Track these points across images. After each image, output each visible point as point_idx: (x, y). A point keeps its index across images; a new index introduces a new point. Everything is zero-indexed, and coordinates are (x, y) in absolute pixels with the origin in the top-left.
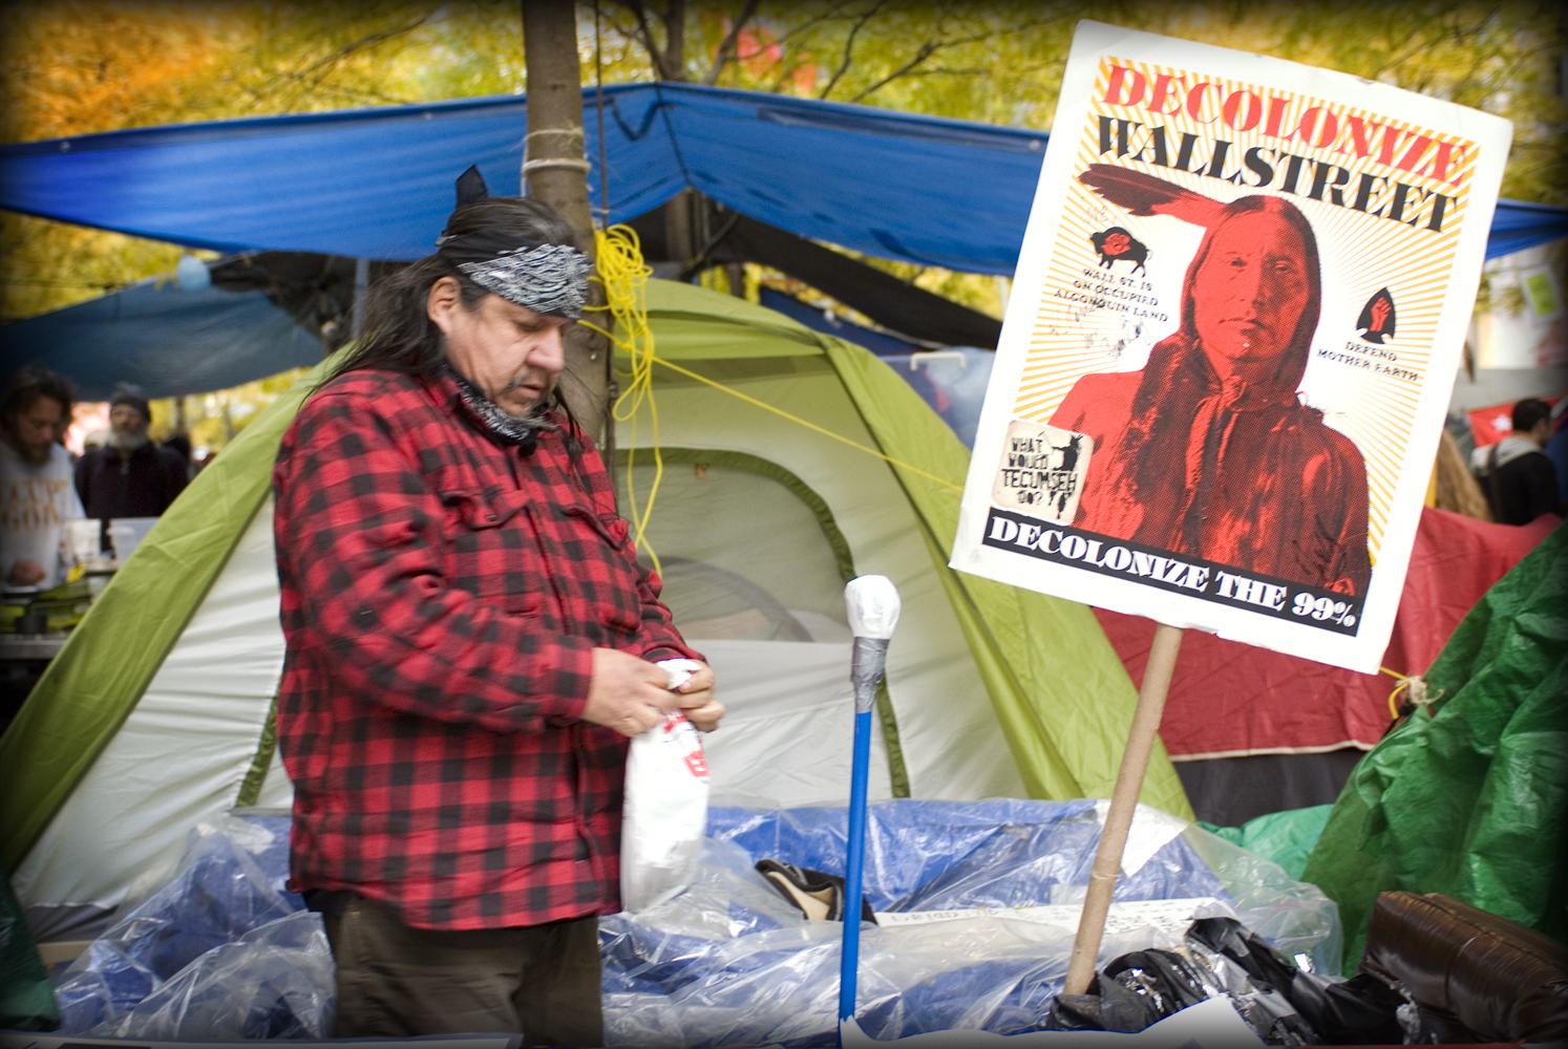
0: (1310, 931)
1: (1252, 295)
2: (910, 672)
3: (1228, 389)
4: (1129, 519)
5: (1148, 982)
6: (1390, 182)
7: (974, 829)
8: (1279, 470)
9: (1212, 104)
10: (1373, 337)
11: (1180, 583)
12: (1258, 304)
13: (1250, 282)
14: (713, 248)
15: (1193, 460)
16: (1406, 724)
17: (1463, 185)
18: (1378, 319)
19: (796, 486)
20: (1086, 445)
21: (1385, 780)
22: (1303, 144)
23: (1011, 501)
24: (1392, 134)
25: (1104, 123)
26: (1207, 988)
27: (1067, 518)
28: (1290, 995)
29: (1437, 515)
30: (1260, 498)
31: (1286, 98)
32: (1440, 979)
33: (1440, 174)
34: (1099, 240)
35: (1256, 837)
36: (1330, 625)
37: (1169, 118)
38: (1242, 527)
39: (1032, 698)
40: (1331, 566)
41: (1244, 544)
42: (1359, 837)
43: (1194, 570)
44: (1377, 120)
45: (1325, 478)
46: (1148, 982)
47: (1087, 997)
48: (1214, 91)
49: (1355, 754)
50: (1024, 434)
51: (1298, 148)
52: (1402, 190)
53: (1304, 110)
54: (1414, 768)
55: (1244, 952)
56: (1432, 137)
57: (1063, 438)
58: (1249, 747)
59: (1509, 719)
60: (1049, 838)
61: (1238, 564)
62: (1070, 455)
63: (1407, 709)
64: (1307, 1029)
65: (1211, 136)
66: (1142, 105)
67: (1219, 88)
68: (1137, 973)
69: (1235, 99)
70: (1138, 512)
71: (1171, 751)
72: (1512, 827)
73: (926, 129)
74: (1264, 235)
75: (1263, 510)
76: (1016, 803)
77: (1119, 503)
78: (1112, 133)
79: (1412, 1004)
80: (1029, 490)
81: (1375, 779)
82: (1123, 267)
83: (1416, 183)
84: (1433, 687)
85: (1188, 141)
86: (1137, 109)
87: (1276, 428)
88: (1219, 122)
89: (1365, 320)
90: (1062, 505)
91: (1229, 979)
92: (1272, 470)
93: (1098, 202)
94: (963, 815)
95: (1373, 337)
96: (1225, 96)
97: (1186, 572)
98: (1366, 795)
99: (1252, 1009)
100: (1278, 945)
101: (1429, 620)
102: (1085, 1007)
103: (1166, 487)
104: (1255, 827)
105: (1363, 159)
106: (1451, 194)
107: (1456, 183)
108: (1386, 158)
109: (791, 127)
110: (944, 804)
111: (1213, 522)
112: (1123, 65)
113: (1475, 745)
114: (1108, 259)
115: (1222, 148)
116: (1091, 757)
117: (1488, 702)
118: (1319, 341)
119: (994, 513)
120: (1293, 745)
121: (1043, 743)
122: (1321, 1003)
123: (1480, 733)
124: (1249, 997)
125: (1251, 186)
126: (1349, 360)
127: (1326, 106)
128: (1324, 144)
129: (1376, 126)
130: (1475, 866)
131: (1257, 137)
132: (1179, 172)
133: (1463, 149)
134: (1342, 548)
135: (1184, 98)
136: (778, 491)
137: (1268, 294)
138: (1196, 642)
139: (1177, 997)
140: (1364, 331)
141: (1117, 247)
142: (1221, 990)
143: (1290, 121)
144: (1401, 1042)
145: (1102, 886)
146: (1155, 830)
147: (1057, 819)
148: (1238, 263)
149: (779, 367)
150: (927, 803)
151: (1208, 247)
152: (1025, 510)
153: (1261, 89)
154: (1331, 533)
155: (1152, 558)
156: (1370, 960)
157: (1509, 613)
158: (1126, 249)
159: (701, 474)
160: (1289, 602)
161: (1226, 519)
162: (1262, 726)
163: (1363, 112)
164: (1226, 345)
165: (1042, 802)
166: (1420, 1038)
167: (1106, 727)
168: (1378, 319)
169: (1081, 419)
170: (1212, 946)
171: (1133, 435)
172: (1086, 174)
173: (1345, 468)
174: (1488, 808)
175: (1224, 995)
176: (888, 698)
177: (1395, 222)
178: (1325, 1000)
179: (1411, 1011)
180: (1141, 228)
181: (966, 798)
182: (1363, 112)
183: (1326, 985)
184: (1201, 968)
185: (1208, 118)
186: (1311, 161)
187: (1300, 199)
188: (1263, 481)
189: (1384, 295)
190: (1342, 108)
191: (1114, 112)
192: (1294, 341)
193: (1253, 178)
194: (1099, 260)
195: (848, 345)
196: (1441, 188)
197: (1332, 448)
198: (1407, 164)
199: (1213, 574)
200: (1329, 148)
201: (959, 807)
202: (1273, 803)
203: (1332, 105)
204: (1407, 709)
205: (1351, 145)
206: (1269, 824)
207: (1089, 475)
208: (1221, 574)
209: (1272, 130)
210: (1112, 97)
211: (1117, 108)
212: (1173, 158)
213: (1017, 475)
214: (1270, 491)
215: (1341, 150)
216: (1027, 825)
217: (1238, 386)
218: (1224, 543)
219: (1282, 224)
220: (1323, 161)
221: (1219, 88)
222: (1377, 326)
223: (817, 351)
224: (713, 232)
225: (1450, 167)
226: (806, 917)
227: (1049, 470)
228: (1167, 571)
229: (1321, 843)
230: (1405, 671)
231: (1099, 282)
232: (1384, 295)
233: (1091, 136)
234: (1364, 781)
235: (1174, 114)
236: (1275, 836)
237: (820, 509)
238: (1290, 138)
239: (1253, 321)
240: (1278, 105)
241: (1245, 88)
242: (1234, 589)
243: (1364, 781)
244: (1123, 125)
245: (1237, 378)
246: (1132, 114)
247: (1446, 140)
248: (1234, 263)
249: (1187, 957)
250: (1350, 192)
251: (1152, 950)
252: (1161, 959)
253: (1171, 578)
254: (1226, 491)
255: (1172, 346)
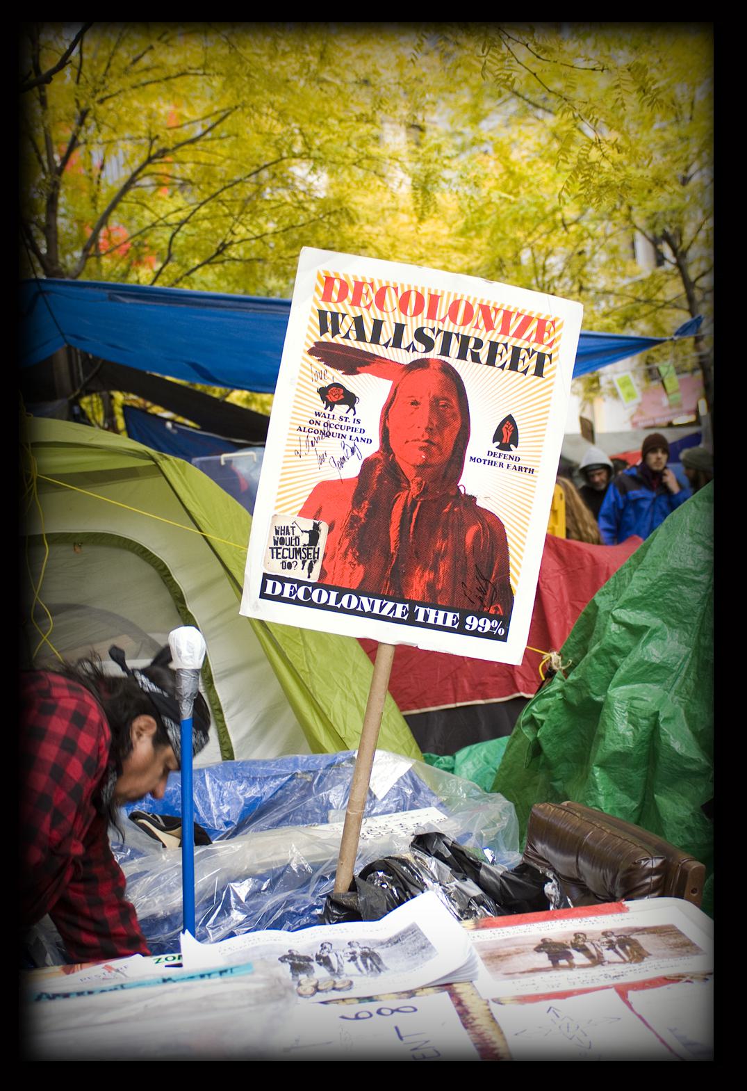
0: (494, 825)
1: (425, 424)
2: (229, 673)
3: (413, 485)
4: (355, 575)
5: (388, 880)
6: (509, 346)
7: (276, 777)
8: (450, 536)
9: (391, 301)
10: (505, 447)
11: (391, 615)
12: (429, 430)
13: (423, 416)
14: (87, 384)
15: (394, 534)
16: (549, 684)
17: (554, 346)
18: (507, 435)
19: (144, 554)
20: (324, 527)
21: (539, 723)
22: (452, 324)
23: (276, 568)
24: (507, 315)
25: (322, 314)
26: (426, 881)
27: (315, 577)
28: (479, 882)
29: (568, 545)
30: (439, 556)
31: (439, 294)
32: (573, 859)
33: (540, 340)
34: (323, 392)
35: (463, 761)
36: (490, 635)
37: (365, 310)
38: (429, 576)
39: (309, 686)
40: (487, 597)
41: (431, 587)
42: (525, 758)
43: (400, 606)
44: (498, 307)
45: (480, 539)
46: (388, 880)
47: (349, 894)
48: (393, 291)
49: (524, 701)
50: (283, 523)
51: (448, 326)
52: (516, 351)
53: (451, 302)
54: (556, 713)
55: (448, 854)
56: (533, 316)
57: (308, 524)
58: (456, 701)
59: (612, 677)
60: (325, 779)
61: (427, 600)
62: (314, 535)
63: (550, 674)
64: (490, 903)
65: (392, 321)
66: (346, 302)
67: (396, 289)
68: (381, 874)
69: (406, 295)
70: (360, 570)
71: (402, 710)
72: (618, 747)
73: (223, 302)
74: (430, 384)
75: (441, 564)
76: (303, 757)
77: (347, 565)
78: (328, 322)
79: (554, 882)
80: (288, 560)
81: (532, 722)
82: (340, 410)
83: (526, 345)
84: (565, 658)
85: (378, 325)
86: (344, 305)
87: (447, 510)
88: (397, 311)
89: (498, 436)
90: (310, 569)
91: (439, 874)
92: (445, 537)
93: (321, 366)
94: (268, 768)
95: (505, 447)
96: (400, 294)
97: (394, 608)
98: (527, 732)
99: (455, 893)
100: (469, 846)
101: (563, 611)
102: (348, 900)
103: (377, 553)
104: (462, 754)
105: (491, 332)
106: (548, 351)
107: (550, 345)
108: (505, 331)
109: (130, 304)
110: (254, 762)
111: (410, 574)
112: (333, 276)
113: (593, 696)
114: (330, 405)
115: (400, 328)
116: (349, 721)
117: (599, 668)
118: (469, 452)
119: (266, 577)
120: (483, 698)
121: (318, 715)
122: (498, 884)
123: (595, 688)
124: (453, 884)
125: (420, 353)
126: (490, 463)
127: (465, 298)
128: (465, 323)
129: (497, 310)
130: (597, 774)
131: (421, 321)
132: (373, 345)
133: (553, 323)
134: (493, 585)
135: (373, 296)
136: (132, 558)
137: (435, 423)
138: (404, 653)
139: (407, 889)
140: (497, 444)
141: (335, 396)
142: (435, 881)
143: (443, 310)
144: (549, 909)
145: (362, 805)
146: (390, 768)
147: (330, 766)
148: (415, 403)
149: (131, 473)
150: (244, 762)
151: (395, 394)
152: (287, 573)
153: (423, 289)
154: (485, 576)
155: (372, 600)
156: (530, 849)
157: (608, 609)
158: (342, 397)
159: (78, 550)
160: (462, 622)
161: (418, 571)
162: (463, 687)
163: (489, 302)
164: (410, 457)
165: (320, 755)
166: (560, 904)
167: (357, 703)
168: (507, 435)
169: (319, 511)
170: (428, 852)
171: (354, 519)
172: (312, 349)
173: (492, 533)
174: (602, 736)
175: (437, 885)
176: (215, 691)
177: (513, 372)
178: (501, 882)
179: (553, 887)
180: (351, 383)
181: (271, 755)
182: (489, 302)
183: (501, 872)
184: (422, 868)
185: (390, 309)
186: (457, 335)
187: (453, 360)
188: (440, 545)
189: (510, 419)
190: (475, 300)
191: (329, 307)
192: (453, 452)
193: (420, 347)
194: (324, 405)
195: (171, 458)
196: (541, 349)
197: (482, 520)
198: (518, 334)
199: (412, 608)
200: (469, 326)
201: (265, 763)
202: (474, 738)
203: (469, 297)
204: (550, 674)
205: (482, 324)
206: (471, 751)
207: (327, 547)
208: (417, 608)
209: (432, 315)
210: (327, 297)
211: (331, 304)
212: (369, 336)
213: (280, 551)
214: (445, 551)
215: (477, 327)
216: (310, 772)
217: (419, 484)
218: (417, 589)
219: (441, 376)
220: (465, 334)
221: (396, 289)
222: (506, 439)
223: (152, 463)
224: (85, 374)
225: (546, 335)
226: (164, 846)
227: (301, 546)
228: (382, 608)
229: (503, 764)
230: (548, 650)
231: (326, 420)
232: (510, 419)
233: (315, 323)
234: (525, 724)
235: (368, 307)
236: (475, 760)
237: (161, 567)
238: (443, 321)
239: (426, 441)
240: (434, 299)
241: (413, 288)
242: (426, 616)
243: (525, 724)
244: (335, 315)
245: (419, 479)
246: (340, 308)
247: (542, 318)
248: (412, 404)
249: (412, 860)
250: (484, 353)
251: (390, 858)
252: (395, 864)
253: (385, 612)
254: (416, 553)
255: (376, 459)
